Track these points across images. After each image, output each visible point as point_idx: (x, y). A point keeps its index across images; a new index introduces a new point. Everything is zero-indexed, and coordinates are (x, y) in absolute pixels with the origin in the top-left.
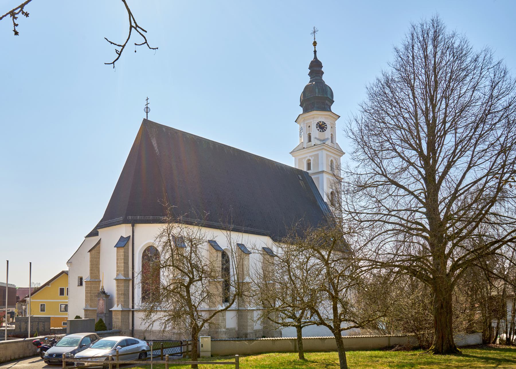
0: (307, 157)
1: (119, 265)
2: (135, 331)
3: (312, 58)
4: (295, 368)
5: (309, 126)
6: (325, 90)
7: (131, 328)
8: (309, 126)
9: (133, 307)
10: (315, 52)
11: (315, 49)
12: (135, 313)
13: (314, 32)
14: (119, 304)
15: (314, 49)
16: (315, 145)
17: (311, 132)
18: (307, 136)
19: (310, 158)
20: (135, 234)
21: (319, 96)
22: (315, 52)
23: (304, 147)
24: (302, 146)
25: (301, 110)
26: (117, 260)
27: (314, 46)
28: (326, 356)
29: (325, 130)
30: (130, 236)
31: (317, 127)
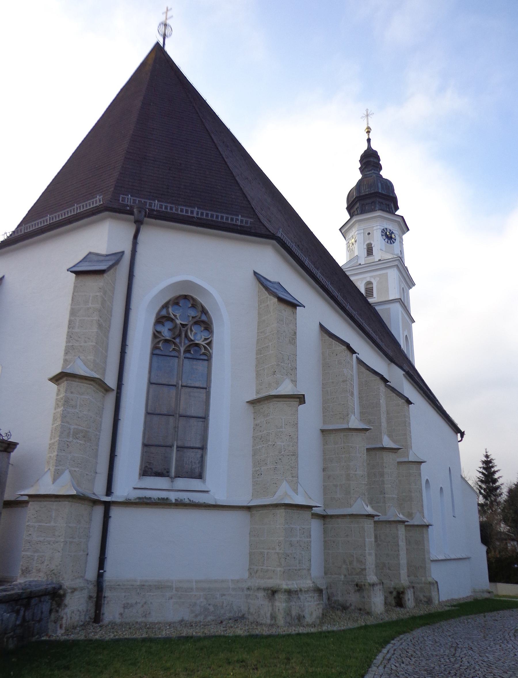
0: (365, 278)
1: (76, 330)
2: (106, 584)
3: (366, 148)
4: (494, 677)
5: (369, 234)
6: (390, 187)
7: (91, 574)
8: (369, 234)
9: (109, 491)
10: (369, 140)
11: (369, 136)
12: (115, 513)
13: (367, 116)
14: (63, 472)
15: (368, 136)
16: (380, 260)
17: (372, 242)
18: (365, 247)
19: (373, 280)
20: (140, 248)
21: (383, 193)
22: (369, 140)
23: (359, 263)
24: (357, 262)
25: (347, 216)
26: (73, 313)
27: (367, 132)
28: (511, 636)
29: (394, 242)
30: (123, 253)
31: (382, 235)
